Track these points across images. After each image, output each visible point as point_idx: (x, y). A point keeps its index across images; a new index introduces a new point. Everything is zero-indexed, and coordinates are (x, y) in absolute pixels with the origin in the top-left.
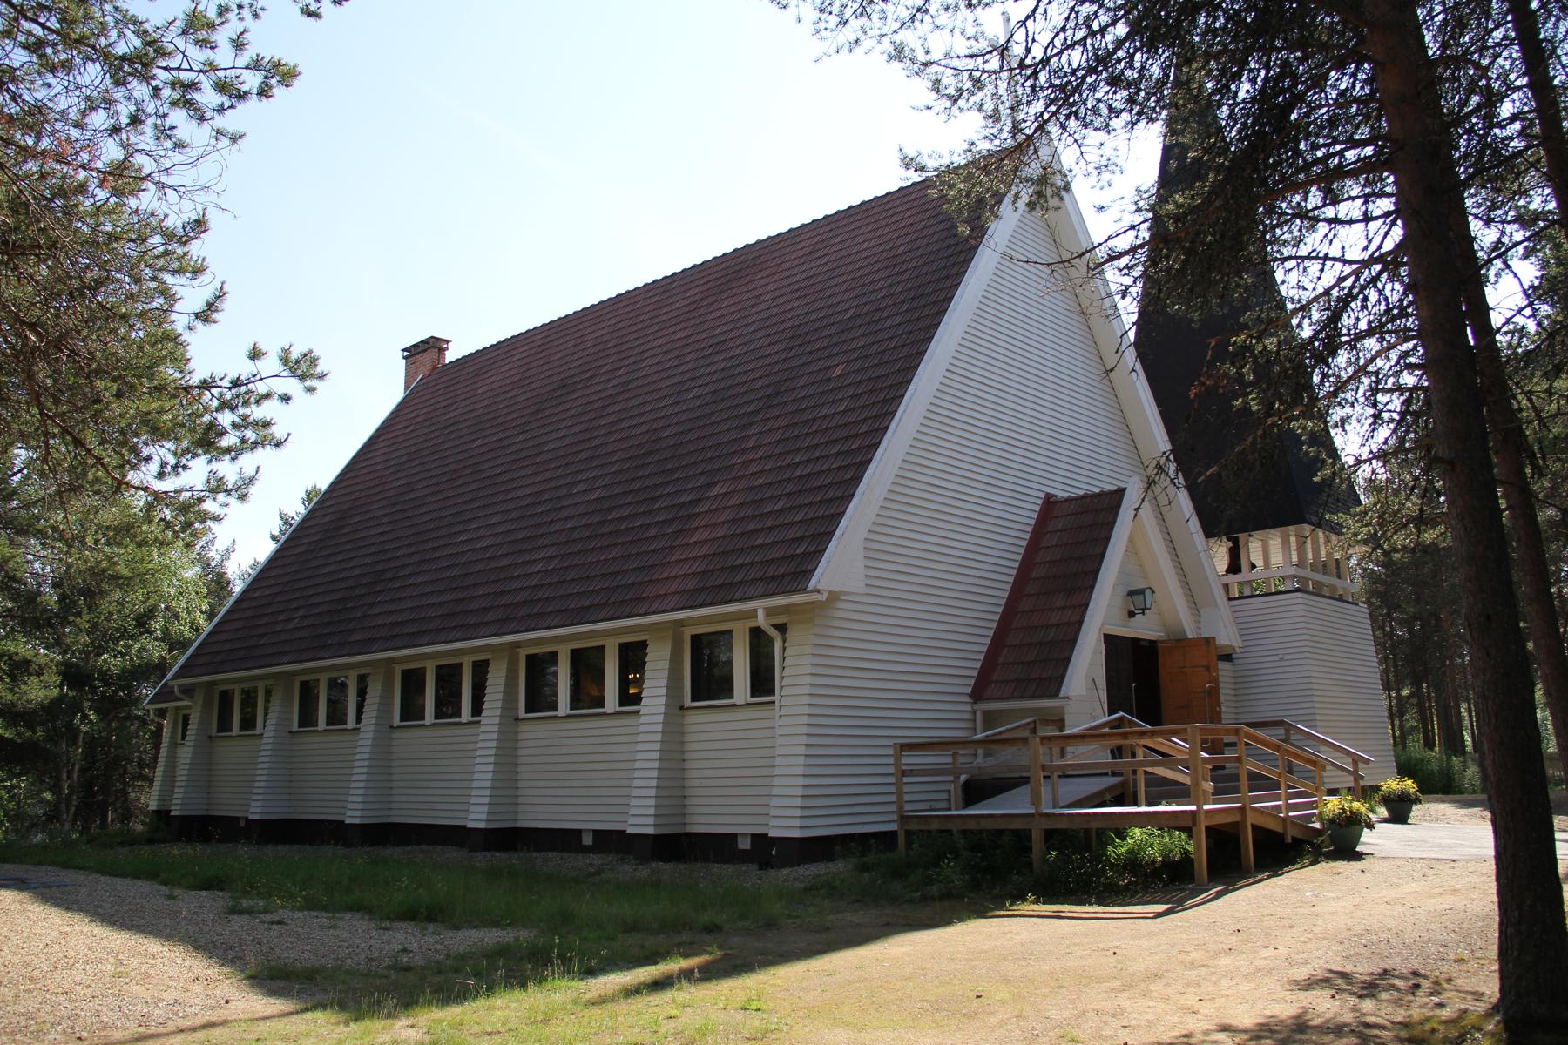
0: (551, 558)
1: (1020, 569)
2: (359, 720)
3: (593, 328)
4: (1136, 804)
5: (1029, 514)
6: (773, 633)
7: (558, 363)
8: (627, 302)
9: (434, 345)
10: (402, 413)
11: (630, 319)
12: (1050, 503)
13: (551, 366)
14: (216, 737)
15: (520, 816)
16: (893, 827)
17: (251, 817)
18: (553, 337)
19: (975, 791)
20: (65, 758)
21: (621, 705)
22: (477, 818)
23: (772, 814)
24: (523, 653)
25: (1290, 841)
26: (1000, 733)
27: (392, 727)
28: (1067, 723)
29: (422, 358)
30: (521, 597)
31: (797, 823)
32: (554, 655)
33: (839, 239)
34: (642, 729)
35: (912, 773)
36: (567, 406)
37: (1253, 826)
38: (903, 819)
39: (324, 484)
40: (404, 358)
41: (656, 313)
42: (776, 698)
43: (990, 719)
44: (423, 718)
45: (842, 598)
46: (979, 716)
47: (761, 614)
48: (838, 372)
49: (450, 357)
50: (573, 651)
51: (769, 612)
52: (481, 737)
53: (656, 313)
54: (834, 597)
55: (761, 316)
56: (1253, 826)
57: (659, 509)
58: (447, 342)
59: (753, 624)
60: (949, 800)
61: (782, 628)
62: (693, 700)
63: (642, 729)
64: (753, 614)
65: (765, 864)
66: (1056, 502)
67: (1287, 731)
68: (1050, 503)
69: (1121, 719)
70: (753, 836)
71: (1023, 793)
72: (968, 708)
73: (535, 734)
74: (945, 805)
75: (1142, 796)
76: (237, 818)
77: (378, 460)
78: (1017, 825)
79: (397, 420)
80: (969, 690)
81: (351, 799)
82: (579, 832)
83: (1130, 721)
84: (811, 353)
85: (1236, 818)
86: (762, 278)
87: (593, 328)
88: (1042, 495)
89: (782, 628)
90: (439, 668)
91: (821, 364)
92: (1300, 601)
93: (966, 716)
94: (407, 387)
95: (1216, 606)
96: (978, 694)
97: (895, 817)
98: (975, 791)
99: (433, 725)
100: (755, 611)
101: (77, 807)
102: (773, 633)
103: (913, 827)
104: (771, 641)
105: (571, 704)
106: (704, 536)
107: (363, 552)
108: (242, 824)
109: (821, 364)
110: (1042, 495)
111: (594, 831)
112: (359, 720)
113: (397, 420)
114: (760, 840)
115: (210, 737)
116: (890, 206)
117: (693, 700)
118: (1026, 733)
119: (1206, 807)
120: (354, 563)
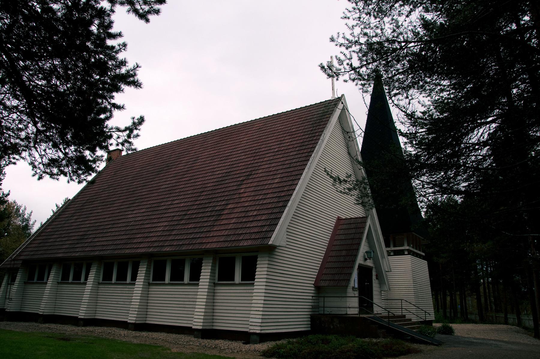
0: (166, 226)
5: (332, 223)
7: (165, 158)
8: (191, 140)
10: (85, 191)
11: (193, 145)
12: (339, 219)
14: (151, 284)
15: (148, 319)
20: (429, 80)
21: (242, 281)
22: (131, 318)
23: (195, 314)
36: (170, 173)
39: (71, 197)
45: (277, 248)
52: (135, 289)
57: (207, 211)
62: (153, 281)
66: (341, 219)
68: (339, 219)
73: (157, 291)
80: (313, 282)
81: (81, 309)
86: (242, 136)
92: (410, 258)
95: (385, 258)
105: (131, 279)
110: (337, 217)
115: (214, 283)
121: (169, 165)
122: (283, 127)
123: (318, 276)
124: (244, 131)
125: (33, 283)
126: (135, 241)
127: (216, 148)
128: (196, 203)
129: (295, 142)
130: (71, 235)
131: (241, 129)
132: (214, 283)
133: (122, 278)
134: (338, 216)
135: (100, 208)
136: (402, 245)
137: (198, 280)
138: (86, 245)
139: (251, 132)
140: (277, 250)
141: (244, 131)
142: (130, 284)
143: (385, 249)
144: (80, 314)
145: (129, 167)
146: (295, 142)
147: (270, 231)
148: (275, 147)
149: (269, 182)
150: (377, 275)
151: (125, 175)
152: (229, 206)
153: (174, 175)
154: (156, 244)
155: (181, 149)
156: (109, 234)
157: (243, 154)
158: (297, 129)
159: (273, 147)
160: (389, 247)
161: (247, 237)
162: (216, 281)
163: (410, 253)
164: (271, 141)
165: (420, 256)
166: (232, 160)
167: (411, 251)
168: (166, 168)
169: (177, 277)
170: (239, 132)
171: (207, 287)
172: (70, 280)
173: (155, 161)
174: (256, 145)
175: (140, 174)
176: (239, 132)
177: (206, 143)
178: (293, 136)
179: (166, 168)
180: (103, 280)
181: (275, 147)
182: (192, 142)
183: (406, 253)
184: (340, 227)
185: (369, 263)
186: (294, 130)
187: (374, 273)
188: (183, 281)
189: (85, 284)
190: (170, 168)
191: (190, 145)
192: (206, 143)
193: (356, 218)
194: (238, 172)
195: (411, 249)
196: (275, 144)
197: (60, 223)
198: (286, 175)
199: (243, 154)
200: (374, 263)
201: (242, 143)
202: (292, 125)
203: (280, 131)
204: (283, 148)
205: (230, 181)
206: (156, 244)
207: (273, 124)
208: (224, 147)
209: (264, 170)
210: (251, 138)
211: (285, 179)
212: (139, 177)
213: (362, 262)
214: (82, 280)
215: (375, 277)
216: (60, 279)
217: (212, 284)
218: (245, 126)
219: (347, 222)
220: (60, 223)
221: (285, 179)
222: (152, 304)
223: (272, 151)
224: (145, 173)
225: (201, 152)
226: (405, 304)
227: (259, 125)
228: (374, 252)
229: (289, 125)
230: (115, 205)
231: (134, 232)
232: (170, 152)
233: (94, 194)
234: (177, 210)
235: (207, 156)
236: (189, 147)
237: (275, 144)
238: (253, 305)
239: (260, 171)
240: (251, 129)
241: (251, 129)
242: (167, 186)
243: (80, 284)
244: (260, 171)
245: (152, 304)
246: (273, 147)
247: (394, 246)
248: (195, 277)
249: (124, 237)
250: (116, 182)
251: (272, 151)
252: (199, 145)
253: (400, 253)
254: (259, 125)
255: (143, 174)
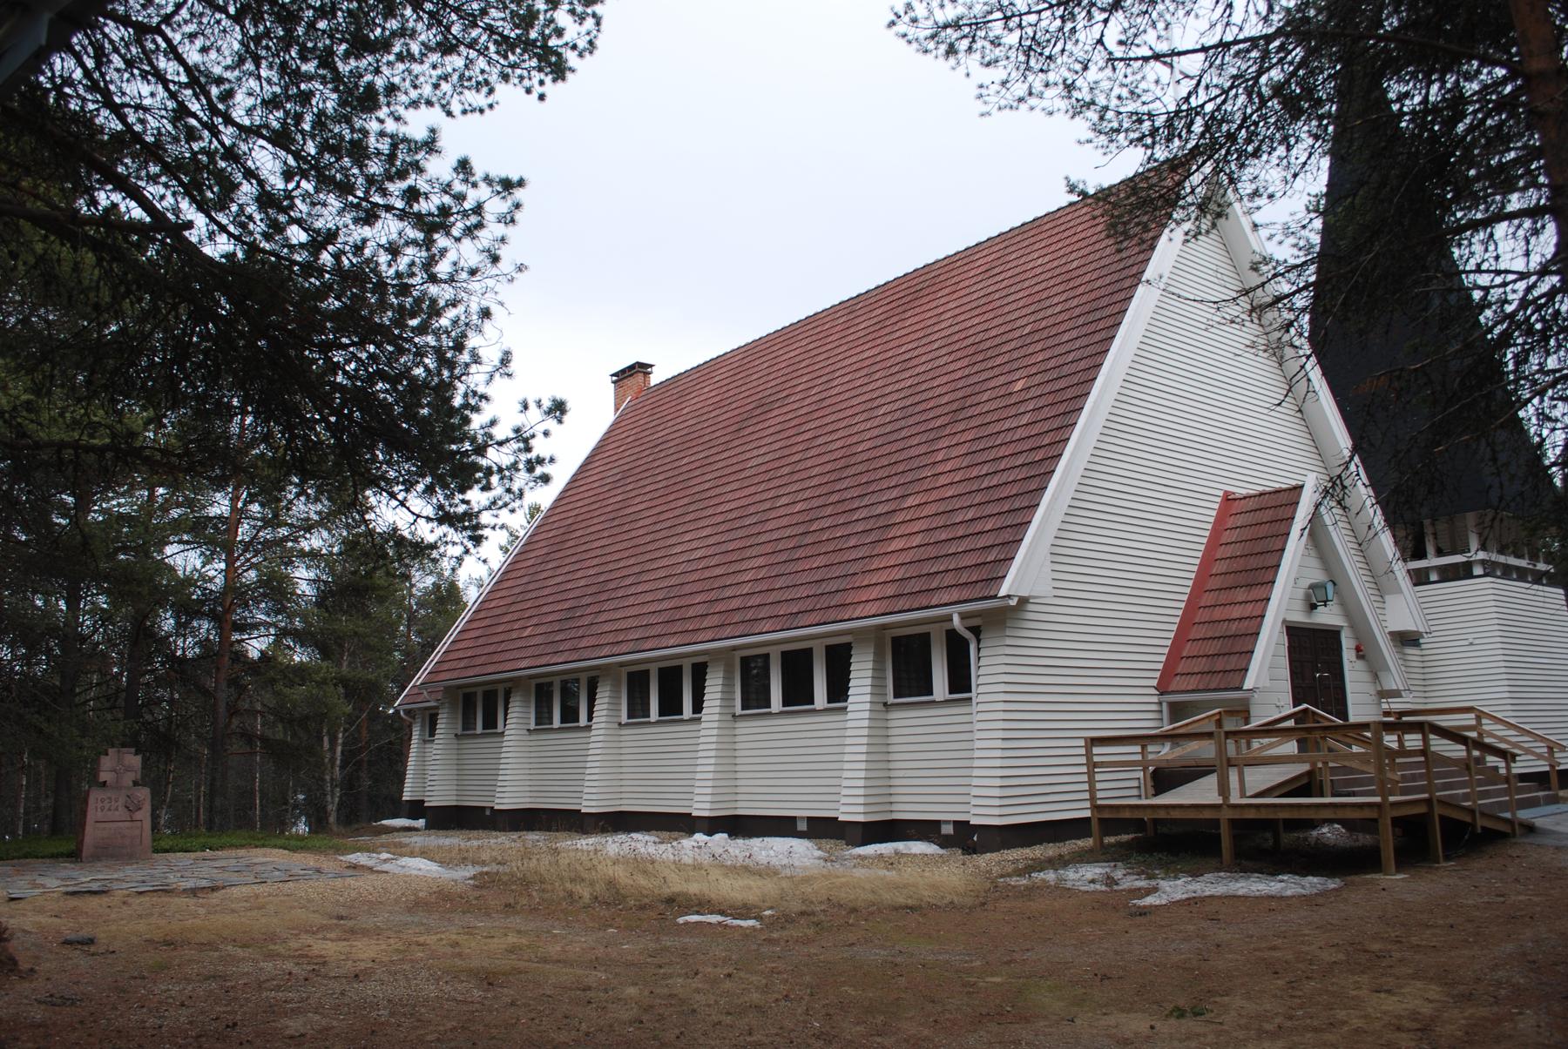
1: (1198, 572)
2: (590, 718)
3: (786, 350)
4: (1322, 795)
6: (968, 635)
7: (755, 384)
9: (640, 369)
12: (1228, 499)
13: (749, 386)
14: (892, 705)
16: (1087, 814)
17: (496, 807)
18: (749, 359)
19: (1164, 779)
21: (829, 702)
24: (534, 682)
25: (1479, 831)
26: (1187, 725)
27: (734, 716)
28: (1252, 714)
29: (629, 382)
30: (735, 603)
31: (861, 809)
32: (551, 684)
33: (1014, 256)
34: (849, 724)
35: (1102, 764)
36: (767, 424)
37: (1442, 817)
38: (1096, 808)
40: (614, 382)
41: (843, 334)
42: (973, 694)
43: (1177, 711)
44: (577, 720)
46: (1165, 707)
47: (956, 619)
48: (1019, 386)
49: (656, 378)
50: (693, 665)
51: (964, 616)
53: (843, 334)
54: (1023, 601)
55: (943, 334)
56: (1442, 817)
58: (651, 366)
59: (947, 626)
60: (1139, 787)
61: (976, 631)
62: (895, 697)
63: (593, 739)
64: (949, 619)
65: (970, 850)
67: (1478, 718)
68: (1228, 499)
69: (1306, 710)
70: (955, 823)
71: (1211, 781)
72: (1155, 699)
73: (911, 722)
74: (1135, 792)
75: (1327, 788)
76: (483, 808)
77: (595, 478)
78: (1207, 815)
79: (610, 440)
80: (1155, 683)
82: (937, 823)
83: (1314, 713)
84: (992, 368)
85: (1422, 809)
87: (786, 350)
88: (1221, 493)
89: (976, 631)
90: (661, 670)
91: (1002, 380)
93: (1154, 707)
94: (617, 409)
96: (1162, 689)
97: (1088, 804)
98: (1164, 779)
99: (658, 722)
100: (951, 615)
101: (340, 797)
102: (968, 635)
103: (1106, 815)
104: (966, 644)
106: (900, 546)
107: (588, 564)
108: (488, 813)
109: (1002, 380)
110: (1221, 494)
111: (955, 822)
112: (590, 718)
113: (610, 440)
114: (962, 826)
115: (885, 704)
116: (1061, 221)
117: (895, 697)
118: (1211, 728)
119: (1392, 799)
120: (579, 574)
121: (763, 401)
122: (1046, 259)
123: (1166, 664)
124: (948, 283)
125: (476, 736)
126: (691, 612)
127: (879, 341)
128: (830, 500)
129: (1075, 302)
130: (545, 609)
131: (941, 278)
132: (734, 716)
133: (671, 706)
134: (1226, 492)
135: (606, 534)
136: (1465, 549)
137: (967, 688)
138: (580, 633)
139: (967, 283)
140: (1030, 607)
141: (948, 283)
142: (691, 720)
143: (1400, 570)
144: (697, 805)
145: (669, 418)
146: (1075, 302)
147: (1005, 560)
148: (1024, 321)
149: (1007, 426)
150: (1358, 649)
151: (660, 441)
152: (910, 501)
153: (778, 428)
154: (737, 617)
155: (792, 354)
156: (631, 601)
157: (944, 351)
158: (1083, 261)
159: (1018, 323)
160: (1420, 554)
161: (949, 580)
162: (891, 699)
163: (1490, 569)
164: (1014, 306)
165: (1538, 578)
166: (917, 370)
167: (1495, 564)
168: (759, 411)
169: (798, 694)
170: (934, 289)
171: (867, 715)
172: (557, 723)
173: (731, 393)
174: (976, 321)
175: (696, 435)
176: (934, 289)
177: (852, 330)
178: (1071, 284)
179: (759, 411)
180: (629, 717)
181: (1024, 321)
182: (819, 329)
183: (1434, 577)
184: (1231, 522)
185: (1328, 616)
186: (1075, 264)
187: (1347, 643)
188: (812, 703)
189: (588, 728)
190: (766, 408)
191: (814, 338)
192: (852, 330)
193: (1262, 494)
194: (931, 404)
195: (1495, 557)
196: (1024, 312)
197: (519, 582)
198: (1050, 399)
199: (944, 351)
200: (1347, 614)
201: (942, 318)
202: (1069, 249)
203: (1039, 270)
204: (1044, 324)
205: (913, 430)
206: (737, 617)
207: (1021, 252)
208: (898, 334)
209: (994, 394)
210: (965, 300)
211: (1045, 413)
212: (694, 443)
213: (1299, 617)
214: (583, 721)
215: (1353, 653)
216: (460, 726)
217: (881, 707)
218: (951, 267)
219: (1251, 504)
220: (519, 582)
221: (1045, 413)
222: (901, 773)
223: (1017, 334)
224: (709, 430)
225: (840, 357)
226: (1487, 725)
227: (985, 260)
228: (1335, 584)
229: (1062, 252)
230: (641, 523)
231: (687, 589)
232: (766, 365)
233: (593, 499)
234: (785, 521)
235: (855, 367)
236: (811, 346)
237: (1024, 312)
238: (701, 754)
239: (985, 397)
240: (966, 276)
241: (966, 276)
242: (760, 460)
243: (579, 729)
244: (985, 397)
245: (901, 773)
246: (1018, 323)
247: (1440, 552)
248: (839, 691)
249: (665, 605)
250: (640, 462)
251: (1017, 334)
252: (837, 336)
253: (1463, 572)
254: (985, 260)
255: (702, 433)
